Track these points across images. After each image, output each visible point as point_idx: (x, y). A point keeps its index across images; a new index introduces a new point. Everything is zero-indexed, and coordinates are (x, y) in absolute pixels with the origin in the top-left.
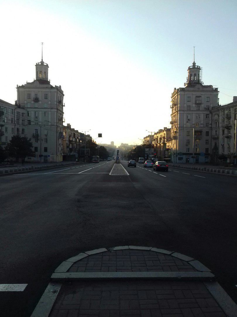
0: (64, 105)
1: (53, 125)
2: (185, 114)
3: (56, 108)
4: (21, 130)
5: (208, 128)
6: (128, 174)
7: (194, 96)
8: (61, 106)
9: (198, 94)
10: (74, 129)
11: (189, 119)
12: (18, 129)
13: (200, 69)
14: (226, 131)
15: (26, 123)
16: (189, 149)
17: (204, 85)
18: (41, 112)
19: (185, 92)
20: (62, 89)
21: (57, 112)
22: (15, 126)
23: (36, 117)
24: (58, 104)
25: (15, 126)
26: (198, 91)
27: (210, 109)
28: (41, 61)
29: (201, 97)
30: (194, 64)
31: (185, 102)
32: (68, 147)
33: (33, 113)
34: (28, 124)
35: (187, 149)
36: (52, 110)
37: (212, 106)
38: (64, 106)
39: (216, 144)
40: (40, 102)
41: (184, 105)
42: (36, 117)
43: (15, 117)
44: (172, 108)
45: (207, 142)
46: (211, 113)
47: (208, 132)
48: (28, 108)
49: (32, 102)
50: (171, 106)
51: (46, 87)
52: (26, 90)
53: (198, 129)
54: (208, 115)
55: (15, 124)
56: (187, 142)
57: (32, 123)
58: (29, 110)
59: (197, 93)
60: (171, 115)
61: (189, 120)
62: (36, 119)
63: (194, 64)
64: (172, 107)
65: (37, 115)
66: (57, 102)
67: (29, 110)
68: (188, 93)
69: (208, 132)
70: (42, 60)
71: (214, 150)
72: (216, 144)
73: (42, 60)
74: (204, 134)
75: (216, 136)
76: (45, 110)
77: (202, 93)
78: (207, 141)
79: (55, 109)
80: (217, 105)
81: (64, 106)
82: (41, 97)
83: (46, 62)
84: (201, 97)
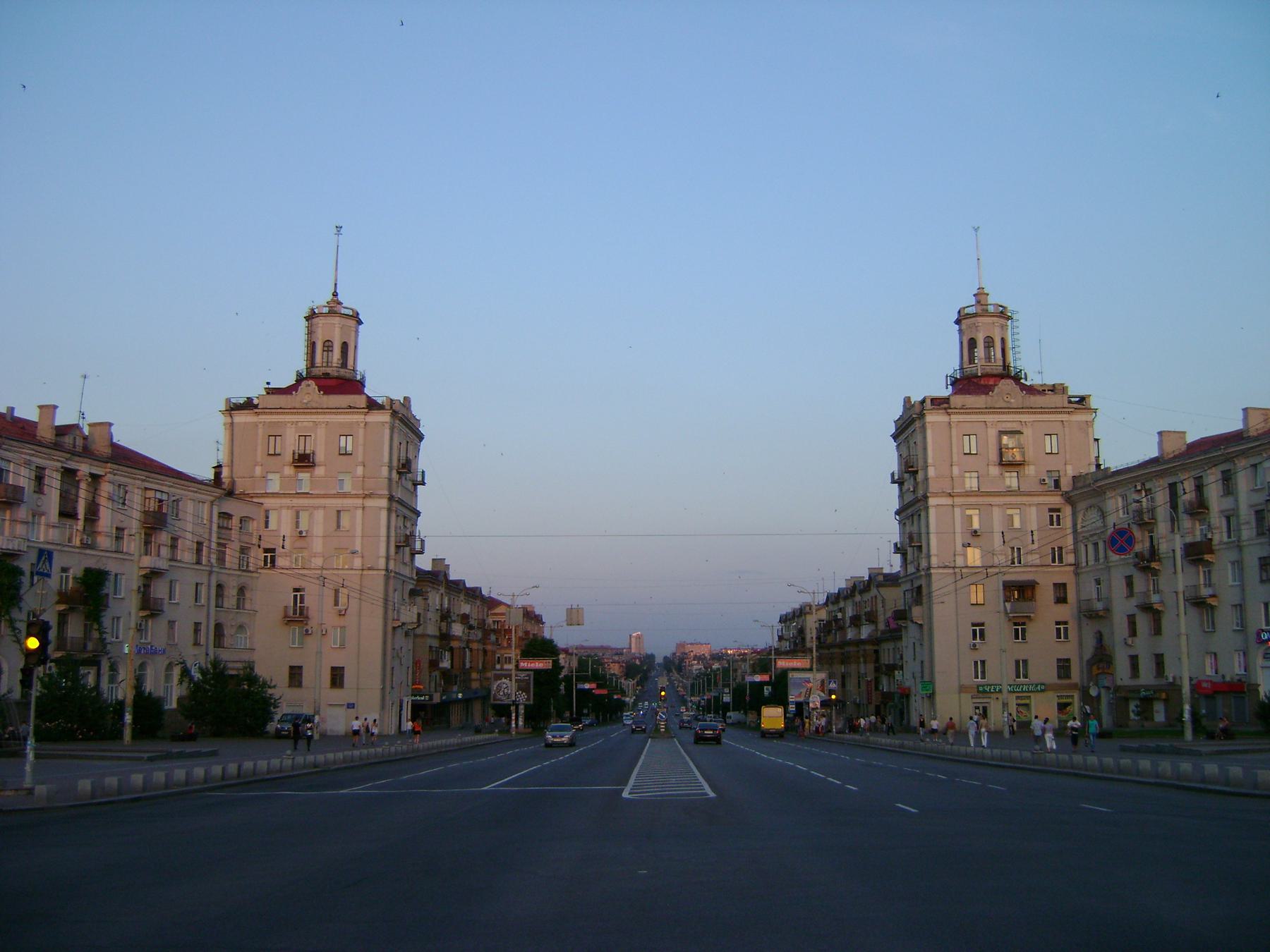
0: (419, 479)
1: (369, 569)
2: (957, 510)
3: (386, 492)
4: (234, 592)
5: (1062, 569)
6: (712, 794)
7: (993, 433)
8: (410, 486)
9: (1010, 421)
10: (464, 582)
11: (975, 532)
12: (220, 587)
13: (1009, 318)
14: (1140, 584)
15: (256, 556)
16: (983, 662)
17: (1028, 383)
18: (319, 515)
19: (949, 414)
20: (416, 410)
21: (389, 510)
22: (211, 573)
23: (301, 532)
24: (395, 475)
25: (211, 573)
26: (1009, 410)
27: (1066, 485)
28: (330, 297)
29: (1019, 432)
30: (980, 296)
31: (955, 459)
32: (434, 664)
33: (287, 516)
34: (266, 563)
35: (976, 663)
36: (370, 503)
37: (1070, 471)
38: (423, 483)
39: (1100, 637)
40: (320, 471)
41: (952, 471)
42: (301, 532)
43: (211, 529)
44: (900, 483)
45: (1061, 630)
46: (1069, 499)
47: (1064, 585)
48: (266, 495)
49: (289, 471)
50: (893, 475)
51: (350, 407)
52: (263, 418)
53: (1012, 624)
54: (1058, 510)
55: (212, 566)
56: (1017, 630)
57: (280, 562)
58: (268, 502)
59: (1004, 417)
60: (898, 513)
61: (975, 533)
62: (300, 543)
63: (980, 296)
64: (896, 477)
65: (303, 526)
66: (391, 468)
67: (268, 502)
68: (965, 416)
69: (1064, 585)
70: (335, 294)
71: (1095, 668)
72: (1100, 637)
73: (335, 294)
74: (1045, 594)
75: (1099, 606)
76: (339, 503)
77: (1024, 418)
78: (1055, 515)
79: (380, 496)
80: (1093, 469)
81: (423, 483)
82: (319, 447)
83: (349, 300)
84: (1019, 432)
